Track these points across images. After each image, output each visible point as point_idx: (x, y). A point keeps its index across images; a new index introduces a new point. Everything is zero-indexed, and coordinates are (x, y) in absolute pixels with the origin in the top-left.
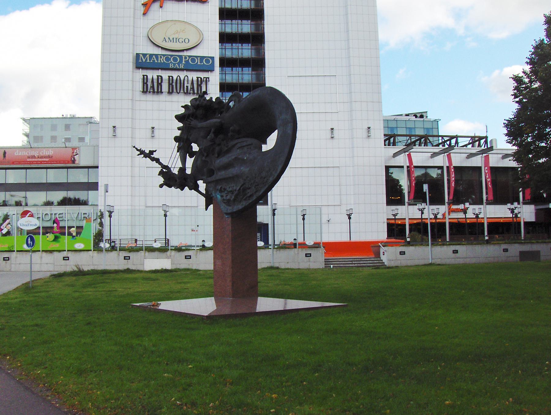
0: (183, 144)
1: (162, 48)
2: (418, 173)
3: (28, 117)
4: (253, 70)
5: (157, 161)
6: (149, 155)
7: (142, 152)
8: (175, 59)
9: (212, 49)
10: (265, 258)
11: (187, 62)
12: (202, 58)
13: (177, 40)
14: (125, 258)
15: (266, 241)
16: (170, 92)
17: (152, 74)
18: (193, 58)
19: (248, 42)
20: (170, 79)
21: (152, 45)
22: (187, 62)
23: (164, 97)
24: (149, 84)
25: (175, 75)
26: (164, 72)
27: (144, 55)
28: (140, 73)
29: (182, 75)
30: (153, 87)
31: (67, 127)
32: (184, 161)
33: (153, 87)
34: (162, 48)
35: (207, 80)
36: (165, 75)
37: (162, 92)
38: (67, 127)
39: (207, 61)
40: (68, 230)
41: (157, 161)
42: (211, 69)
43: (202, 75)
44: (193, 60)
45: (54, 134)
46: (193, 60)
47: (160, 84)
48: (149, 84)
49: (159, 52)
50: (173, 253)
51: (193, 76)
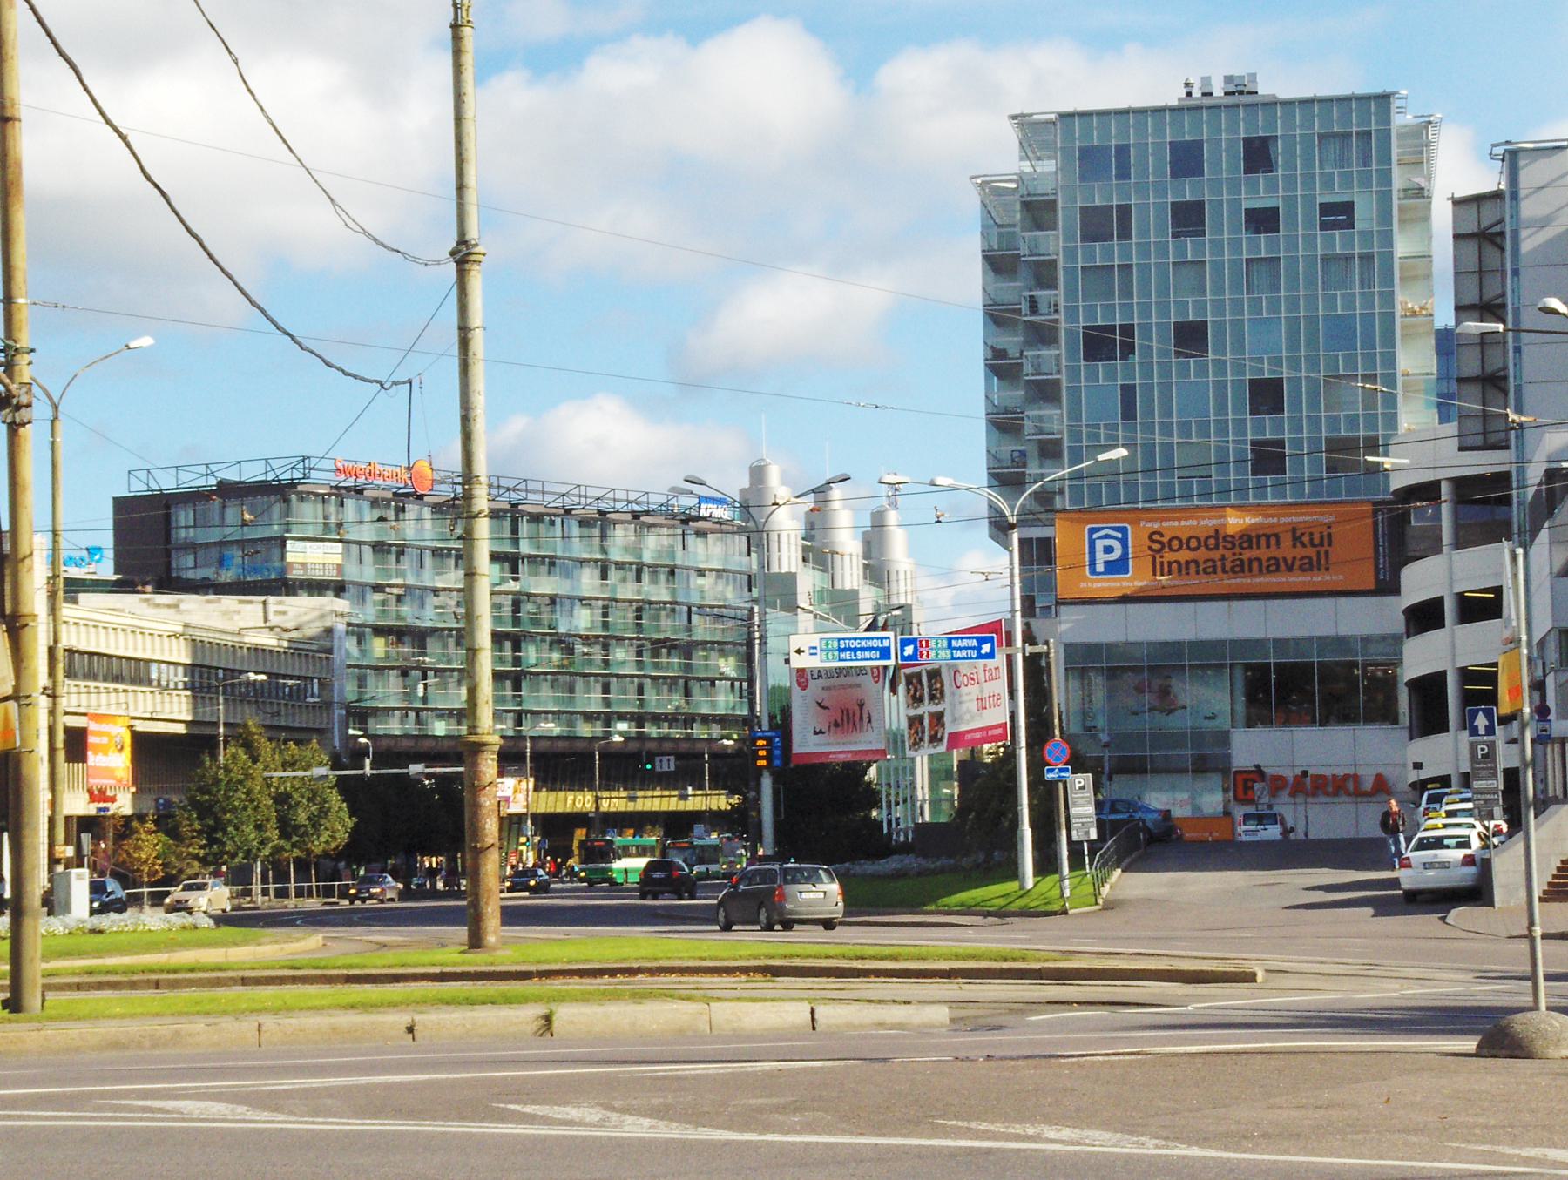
3: (1459, 194)
38: (1258, 155)
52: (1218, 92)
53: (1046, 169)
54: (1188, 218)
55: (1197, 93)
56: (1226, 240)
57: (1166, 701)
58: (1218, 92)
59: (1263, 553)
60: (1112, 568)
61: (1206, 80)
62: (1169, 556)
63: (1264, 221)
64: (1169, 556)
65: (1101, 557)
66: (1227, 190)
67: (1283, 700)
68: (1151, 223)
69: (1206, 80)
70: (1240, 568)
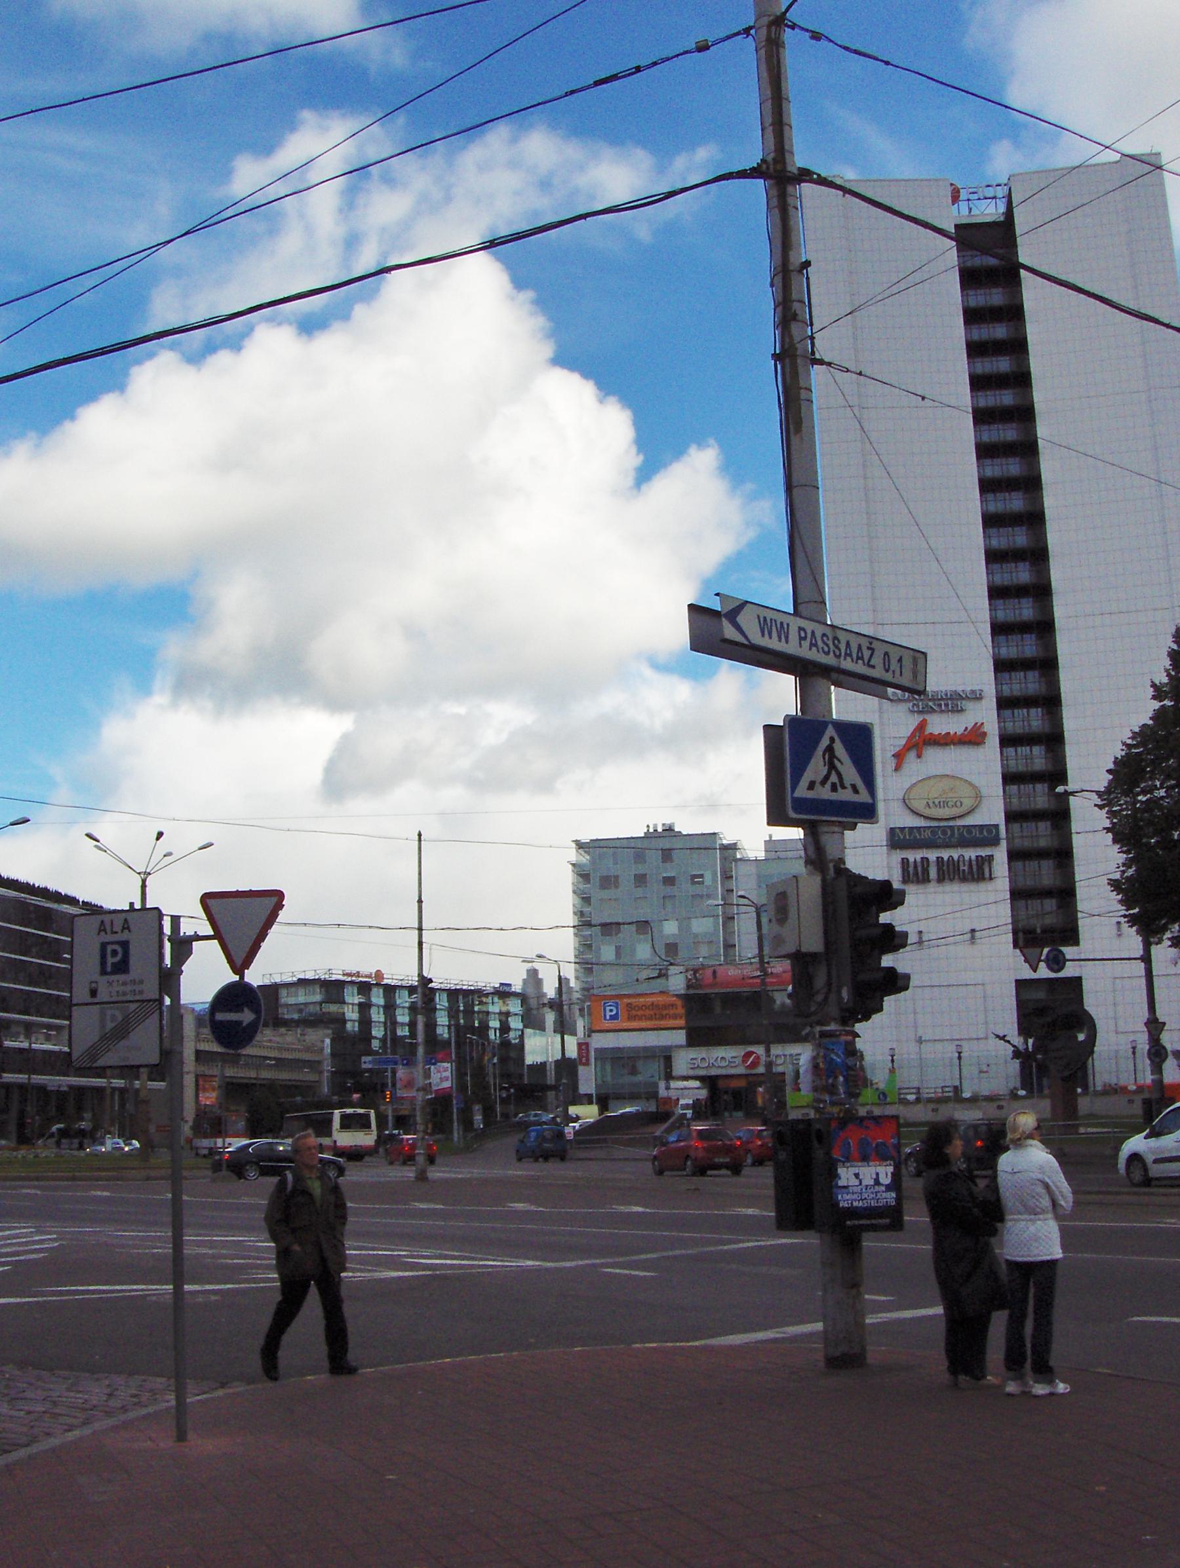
0: (1024, 1031)
1: (926, 818)
2: (922, 1167)
3: (586, 838)
4: (1041, 675)
5: (1008, 1042)
6: (1003, 1038)
7: (998, 1036)
8: (944, 833)
9: (993, 813)
10: (1084, 1104)
11: (961, 835)
12: (982, 827)
13: (945, 804)
14: (933, 1110)
15: (1085, 1087)
16: (941, 880)
17: (914, 856)
18: (969, 828)
19: (1024, 560)
20: (939, 860)
21: (908, 811)
22: (961, 835)
23: (932, 887)
24: (911, 869)
25: (945, 854)
26: (930, 851)
27: (902, 829)
28: (898, 855)
29: (955, 854)
30: (916, 874)
31: (667, 855)
32: (1026, 1043)
33: (916, 874)
34: (926, 818)
35: (990, 858)
36: (932, 855)
37: (929, 881)
38: (667, 855)
39: (990, 832)
40: (19, 1022)
41: (1008, 1042)
42: (994, 842)
43: (984, 852)
44: (970, 832)
45: (641, 869)
46: (970, 832)
47: (926, 871)
48: (911, 869)
49: (921, 823)
50: (984, 1104)
51: (971, 853)
52: (660, 830)
53: (868, 1172)
54: (641, 879)
55: (651, 830)
56: (655, 889)
57: (634, 1071)
58: (660, 830)
59: (672, 1012)
60: (613, 1018)
61: (655, 826)
62: (634, 1013)
63: (669, 881)
64: (634, 1013)
65: (608, 1014)
66: (653, 865)
67: (581, 875)
68: (627, 882)
69: (655, 826)
70: (663, 1017)
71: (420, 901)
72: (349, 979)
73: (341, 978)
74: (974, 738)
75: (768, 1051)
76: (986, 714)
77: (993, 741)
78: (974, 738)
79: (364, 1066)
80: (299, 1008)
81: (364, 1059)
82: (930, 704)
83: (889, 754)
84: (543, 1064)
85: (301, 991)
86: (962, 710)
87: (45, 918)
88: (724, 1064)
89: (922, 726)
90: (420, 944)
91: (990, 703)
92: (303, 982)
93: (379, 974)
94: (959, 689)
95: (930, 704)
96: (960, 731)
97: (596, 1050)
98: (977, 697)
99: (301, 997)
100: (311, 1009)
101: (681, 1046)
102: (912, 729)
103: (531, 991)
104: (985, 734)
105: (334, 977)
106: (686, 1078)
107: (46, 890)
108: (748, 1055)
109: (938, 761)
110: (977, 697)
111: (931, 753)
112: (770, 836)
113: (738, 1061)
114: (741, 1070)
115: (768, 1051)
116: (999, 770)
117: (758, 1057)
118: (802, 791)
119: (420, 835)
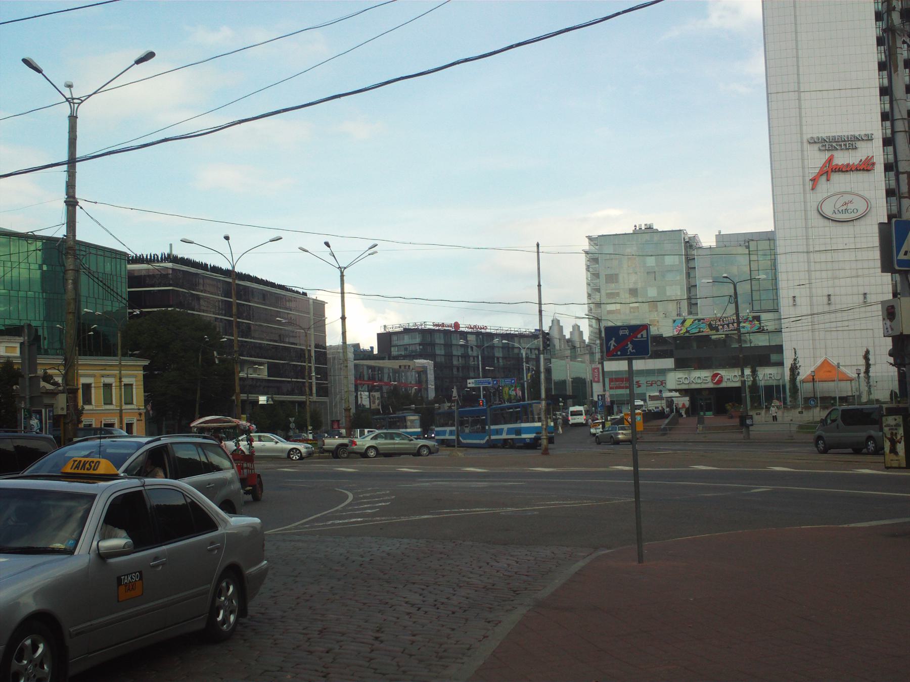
3: (595, 234)
71: (539, 286)
72: (470, 330)
73: (432, 327)
74: (866, 166)
75: (754, 372)
76: (876, 151)
77: (880, 168)
78: (866, 166)
79: (469, 386)
80: (405, 347)
81: (469, 381)
82: (834, 144)
83: (807, 179)
84: (564, 382)
85: (406, 337)
86: (856, 148)
87: (244, 293)
88: (699, 381)
89: (830, 159)
90: (540, 311)
91: (878, 142)
92: (407, 331)
93: (457, 325)
94: (857, 134)
95: (834, 144)
96: (857, 162)
97: (269, 376)
98: (869, 138)
99: (407, 340)
100: (411, 348)
101: (670, 370)
102: (823, 161)
103: (576, 338)
104: (873, 164)
105: (428, 327)
106: (671, 391)
107: (249, 276)
108: (715, 375)
109: (840, 182)
110: (869, 138)
111: (836, 177)
112: (720, 232)
113: (709, 379)
114: (711, 385)
115: (754, 372)
116: (884, 188)
117: (722, 377)
118: (901, 256)
119: (538, 245)
